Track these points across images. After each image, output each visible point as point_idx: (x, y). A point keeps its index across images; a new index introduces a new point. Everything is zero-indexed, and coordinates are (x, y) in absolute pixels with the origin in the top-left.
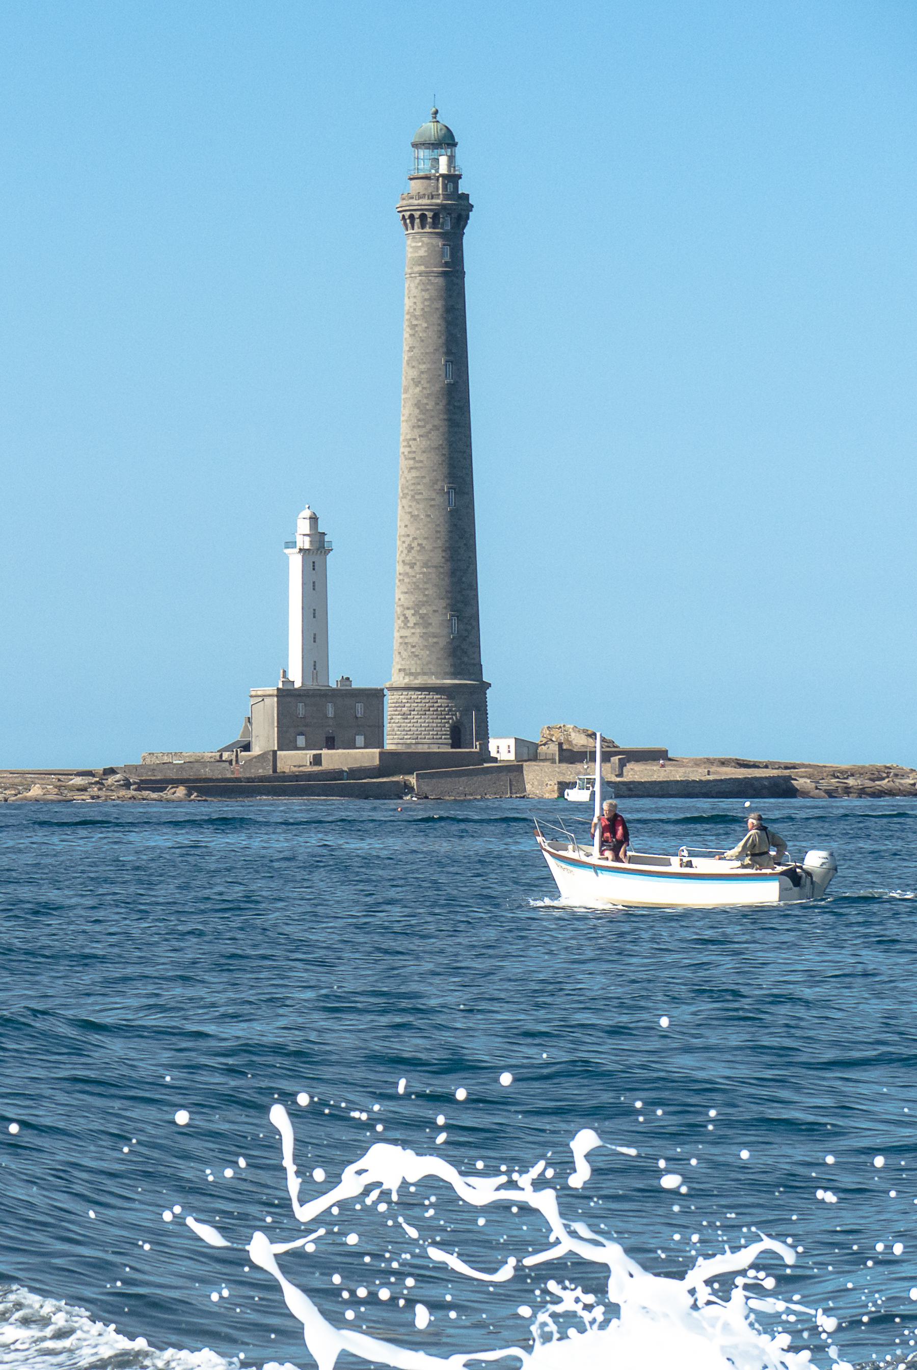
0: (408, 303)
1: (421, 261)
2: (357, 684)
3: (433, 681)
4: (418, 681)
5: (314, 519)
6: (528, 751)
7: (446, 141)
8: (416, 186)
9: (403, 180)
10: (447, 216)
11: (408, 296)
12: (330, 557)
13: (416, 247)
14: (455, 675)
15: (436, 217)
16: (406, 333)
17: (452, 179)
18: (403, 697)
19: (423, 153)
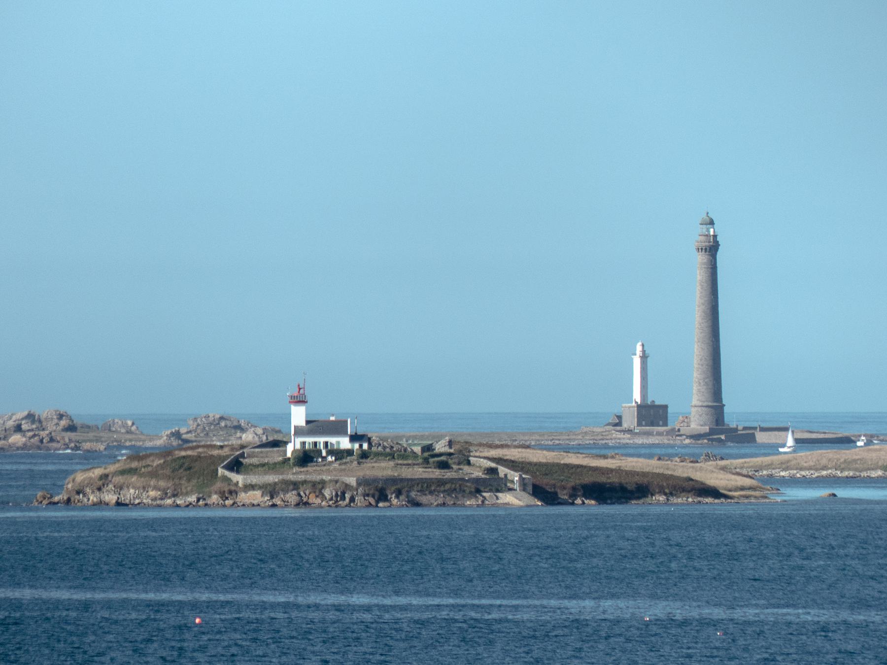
0: (699, 277)
1: (704, 264)
2: (657, 403)
3: (710, 404)
4: (705, 404)
5: (643, 345)
6: (484, 497)
7: (712, 223)
8: (703, 238)
9: (695, 235)
10: (712, 249)
11: (699, 275)
12: (649, 359)
13: (701, 259)
14: (715, 402)
15: (710, 248)
16: (698, 288)
17: (715, 236)
18: (696, 409)
19: (704, 226)
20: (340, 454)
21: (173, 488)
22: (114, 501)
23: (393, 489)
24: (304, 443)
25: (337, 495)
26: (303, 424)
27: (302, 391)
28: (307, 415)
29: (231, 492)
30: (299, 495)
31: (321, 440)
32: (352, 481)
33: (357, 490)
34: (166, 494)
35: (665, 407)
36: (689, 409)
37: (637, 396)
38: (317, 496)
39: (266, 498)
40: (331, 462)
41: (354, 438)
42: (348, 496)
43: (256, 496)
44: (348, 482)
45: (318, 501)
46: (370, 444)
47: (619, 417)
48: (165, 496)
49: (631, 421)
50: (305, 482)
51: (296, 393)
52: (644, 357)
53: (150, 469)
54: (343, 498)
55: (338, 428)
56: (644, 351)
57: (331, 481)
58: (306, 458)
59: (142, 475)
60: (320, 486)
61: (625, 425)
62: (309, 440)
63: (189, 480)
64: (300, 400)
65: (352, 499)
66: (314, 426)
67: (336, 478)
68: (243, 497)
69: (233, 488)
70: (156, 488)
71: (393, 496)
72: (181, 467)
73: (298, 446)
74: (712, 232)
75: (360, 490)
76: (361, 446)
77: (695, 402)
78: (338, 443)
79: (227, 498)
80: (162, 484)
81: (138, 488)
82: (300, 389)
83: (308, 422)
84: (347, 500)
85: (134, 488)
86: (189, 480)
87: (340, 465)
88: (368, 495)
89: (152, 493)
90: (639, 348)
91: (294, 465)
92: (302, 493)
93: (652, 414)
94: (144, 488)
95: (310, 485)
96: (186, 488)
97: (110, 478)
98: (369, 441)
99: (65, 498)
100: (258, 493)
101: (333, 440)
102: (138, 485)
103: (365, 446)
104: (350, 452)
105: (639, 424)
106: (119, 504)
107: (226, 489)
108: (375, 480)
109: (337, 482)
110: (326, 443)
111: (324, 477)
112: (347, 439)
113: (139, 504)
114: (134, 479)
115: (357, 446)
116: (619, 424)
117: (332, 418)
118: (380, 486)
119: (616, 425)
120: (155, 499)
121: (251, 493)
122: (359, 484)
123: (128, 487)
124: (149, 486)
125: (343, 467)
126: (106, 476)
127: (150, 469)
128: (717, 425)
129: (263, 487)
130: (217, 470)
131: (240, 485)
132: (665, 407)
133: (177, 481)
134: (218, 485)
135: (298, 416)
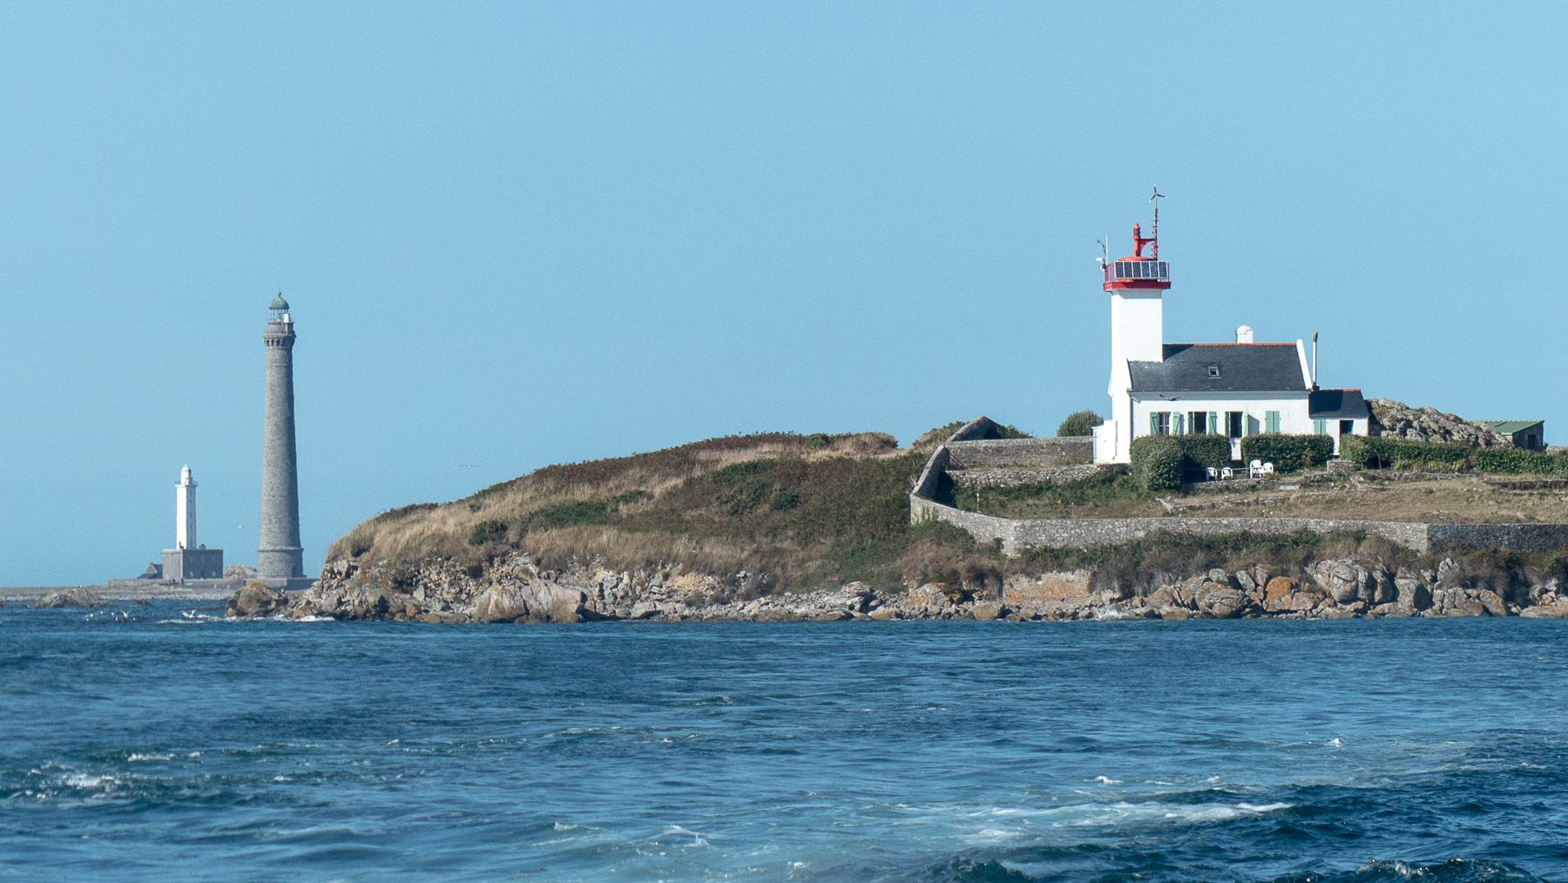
0: (269, 379)
7: (286, 307)
8: (275, 327)
9: (263, 325)
10: (286, 342)
13: (273, 354)
17: (290, 325)
20: (1290, 454)
21: (755, 562)
22: (573, 607)
23: (1549, 560)
24: (1161, 419)
25: (1371, 584)
26: (1157, 356)
27: (1147, 251)
28: (1164, 337)
29: (979, 576)
30: (1234, 583)
31: (1218, 409)
32: (1416, 537)
33: (1433, 565)
34: (735, 582)
35: (219, 553)
36: (251, 554)
37: (182, 538)
38: (1295, 588)
39: (1107, 595)
40: (1270, 483)
41: (1323, 403)
42: (1406, 584)
43: (1065, 591)
44: (1397, 538)
45: (1302, 603)
46: (1374, 423)
47: (159, 567)
48: (729, 589)
49: (173, 570)
50: (1242, 541)
51: (1127, 253)
52: (191, 487)
53: (643, 506)
54: (1392, 594)
55: (1270, 369)
56: (190, 479)
57: (1336, 535)
58: (1185, 464)
59: (629, 525)
60: (1301, 553)
61: (167, 577)
62: (1182, 408)
63: (805, 540)
64: (1143, 279)
65: (1423, 599)
66: (1187, 367)
67: (1357, 524)
68: (1024, 593)
69: (987, 562)
70: (694, 565)
71: (1552, 584)
72: (759, 495)
73: (1144, 429)
74: (286, 320)
75: (1446, 564)
76: (1346, 427)
77: (263, 545)
78: (1273, 417)
79: (967, 596)
80: (716, 550)
81: (630, 567)
82: (1141, 242)
83: (1170, 351)
84: (1406, 601)
85: (608, 565)
86: (805, 540)
87: (1305, 485)
88: (1474, 583)
89: (686, 583)
90: (184, 475)
91: (1156, 488)
92: (1242, 576)
93: (202, 562)
94: (650, 564)
95: (1263, 550)
96: (801, 564)
97: (512, 535)
98: (1367, 409)
99: (372, 600)
100: (1077, 579)
101: (1256, 409)
102: (628, 554)
103: (1360, 427)
104: (1319, 449)
105: (186, 575)
106: (586, 615)
107: (962, 566)
108: (1488, 531)
109: (1359, 537)
110: (1235, 418)
111: (1312, 524)
112: (1303, 404)
113: (648, 615)
114: (607, 536)
115: (1332, 427)
116: (159, 575)
117: (1245, 336)
118: (1504, 549)
119: (154, 576)
120: (695, 601)
121: (1050, 578)
122: (1437, 547)
123: (586, 564)
124: (671, 559)
125: (1314, 493)
126: (499, 528)
127: (643, 506)
128: (294, 574)
129: (1096, 560)
130: (906, 505)
131: (1010, 551)
132: (219, 553)
133: (765, 542)
134: (926, 552)
135: (1138, 329)
